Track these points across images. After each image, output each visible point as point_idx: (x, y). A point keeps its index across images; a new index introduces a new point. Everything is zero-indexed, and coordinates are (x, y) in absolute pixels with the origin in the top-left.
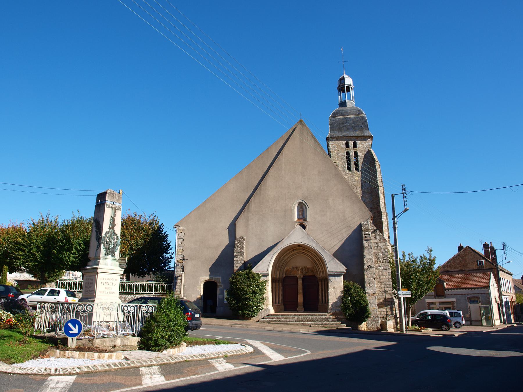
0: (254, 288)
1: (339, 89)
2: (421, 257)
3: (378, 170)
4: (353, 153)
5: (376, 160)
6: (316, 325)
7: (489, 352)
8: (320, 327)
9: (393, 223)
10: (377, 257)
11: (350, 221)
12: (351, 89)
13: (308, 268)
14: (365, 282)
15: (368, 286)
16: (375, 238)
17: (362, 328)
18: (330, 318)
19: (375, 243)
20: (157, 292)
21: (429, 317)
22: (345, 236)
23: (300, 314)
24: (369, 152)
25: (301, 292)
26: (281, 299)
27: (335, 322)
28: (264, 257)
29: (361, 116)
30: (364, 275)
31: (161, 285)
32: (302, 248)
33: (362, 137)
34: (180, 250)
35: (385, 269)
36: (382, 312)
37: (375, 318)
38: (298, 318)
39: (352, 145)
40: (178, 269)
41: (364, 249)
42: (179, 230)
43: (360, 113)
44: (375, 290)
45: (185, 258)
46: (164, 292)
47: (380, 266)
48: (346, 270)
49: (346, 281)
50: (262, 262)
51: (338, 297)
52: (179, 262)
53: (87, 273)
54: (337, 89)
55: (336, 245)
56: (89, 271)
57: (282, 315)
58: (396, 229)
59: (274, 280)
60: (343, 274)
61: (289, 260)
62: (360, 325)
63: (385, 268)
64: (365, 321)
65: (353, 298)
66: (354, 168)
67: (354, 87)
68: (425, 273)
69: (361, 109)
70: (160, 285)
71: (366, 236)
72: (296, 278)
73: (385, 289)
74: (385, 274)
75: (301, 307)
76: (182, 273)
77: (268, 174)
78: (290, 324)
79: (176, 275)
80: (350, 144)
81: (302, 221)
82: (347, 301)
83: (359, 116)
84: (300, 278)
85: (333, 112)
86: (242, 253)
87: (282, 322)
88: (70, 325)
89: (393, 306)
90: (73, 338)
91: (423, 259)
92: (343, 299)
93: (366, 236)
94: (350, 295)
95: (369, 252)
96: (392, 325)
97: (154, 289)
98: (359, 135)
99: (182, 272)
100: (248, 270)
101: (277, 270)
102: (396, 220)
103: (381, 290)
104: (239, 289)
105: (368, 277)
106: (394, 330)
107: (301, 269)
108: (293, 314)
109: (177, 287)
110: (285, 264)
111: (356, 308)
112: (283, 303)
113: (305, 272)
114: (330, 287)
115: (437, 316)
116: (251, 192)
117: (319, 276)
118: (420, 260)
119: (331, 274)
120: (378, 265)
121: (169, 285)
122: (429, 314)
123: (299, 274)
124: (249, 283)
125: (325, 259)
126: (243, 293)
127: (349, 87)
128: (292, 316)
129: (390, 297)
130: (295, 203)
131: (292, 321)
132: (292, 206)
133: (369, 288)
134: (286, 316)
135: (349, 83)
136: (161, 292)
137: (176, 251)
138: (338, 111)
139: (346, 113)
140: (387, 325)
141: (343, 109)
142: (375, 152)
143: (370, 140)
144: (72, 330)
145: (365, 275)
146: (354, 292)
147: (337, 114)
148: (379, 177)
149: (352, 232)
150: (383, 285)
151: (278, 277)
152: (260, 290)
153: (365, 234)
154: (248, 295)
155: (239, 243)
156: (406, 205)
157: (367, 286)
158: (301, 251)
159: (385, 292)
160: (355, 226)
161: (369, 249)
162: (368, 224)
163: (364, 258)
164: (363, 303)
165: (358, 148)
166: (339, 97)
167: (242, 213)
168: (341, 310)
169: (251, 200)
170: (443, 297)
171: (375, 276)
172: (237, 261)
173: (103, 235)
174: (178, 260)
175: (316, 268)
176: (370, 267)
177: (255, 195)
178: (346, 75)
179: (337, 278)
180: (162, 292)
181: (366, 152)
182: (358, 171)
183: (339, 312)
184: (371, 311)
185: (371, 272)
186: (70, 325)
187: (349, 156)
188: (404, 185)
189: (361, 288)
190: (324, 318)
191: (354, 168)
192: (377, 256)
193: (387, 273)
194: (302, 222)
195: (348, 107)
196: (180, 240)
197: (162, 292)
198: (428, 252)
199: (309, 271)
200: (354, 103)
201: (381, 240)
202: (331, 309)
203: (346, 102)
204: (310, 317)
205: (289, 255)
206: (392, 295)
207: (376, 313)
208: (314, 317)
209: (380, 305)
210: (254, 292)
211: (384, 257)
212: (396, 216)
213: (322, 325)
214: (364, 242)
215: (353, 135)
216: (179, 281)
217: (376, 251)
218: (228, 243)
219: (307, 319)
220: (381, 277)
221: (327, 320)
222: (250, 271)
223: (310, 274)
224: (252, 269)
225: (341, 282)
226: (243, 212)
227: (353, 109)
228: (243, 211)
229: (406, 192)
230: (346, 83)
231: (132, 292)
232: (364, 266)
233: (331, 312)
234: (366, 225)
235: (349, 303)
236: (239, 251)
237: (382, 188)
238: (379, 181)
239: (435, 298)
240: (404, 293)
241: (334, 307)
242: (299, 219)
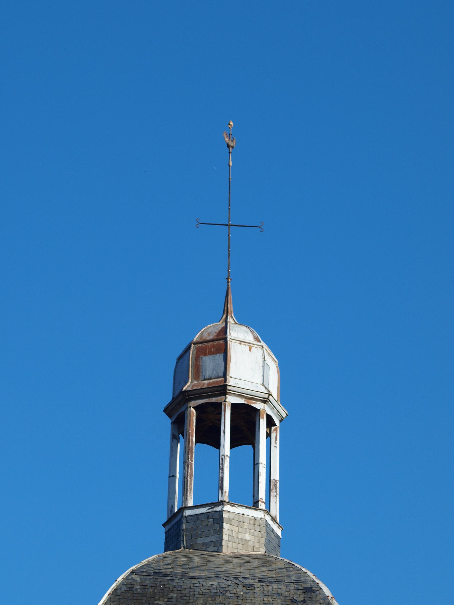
7: (218, 329)
12: (263, 423)
85: (120, 579)
138: (157, 574)
141: (197, 568)
178: (241, 322)
227: (262, 573)
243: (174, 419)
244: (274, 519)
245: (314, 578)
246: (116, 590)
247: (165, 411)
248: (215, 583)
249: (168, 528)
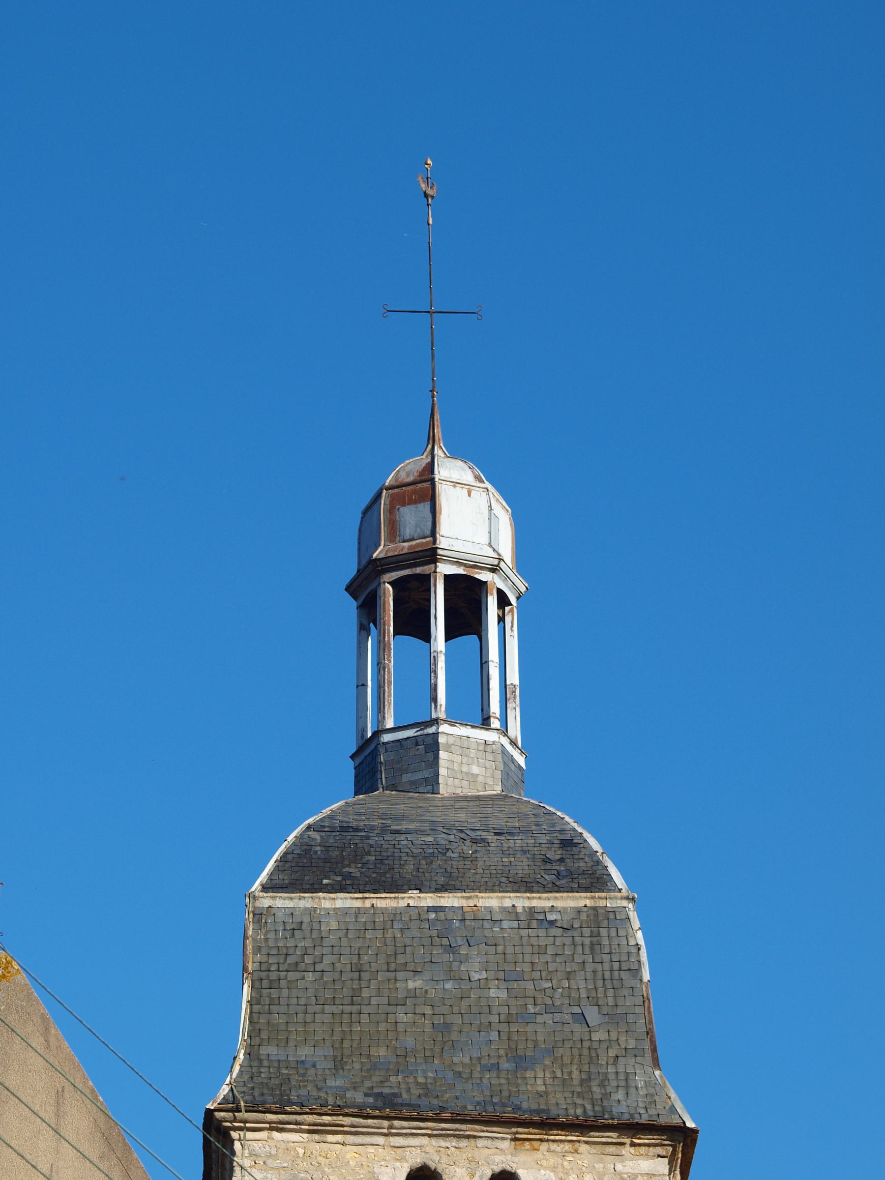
12: (492, 602)
29: (579, 911)
43: (570, 874)
85: (291, 838)
97: (364, 685)
108: (337, 1122)
127: (483, 584)
138: (344, 829)
178: (454, 454)
195: (457, 799)
218: (235, 1147)
227: (499, 821)
243: (362, 598)
244: (513, 743)
245: (575, 825)
246: (285, 854)
247: (347, 589)
248: (430, 839)
249: (358, 760)
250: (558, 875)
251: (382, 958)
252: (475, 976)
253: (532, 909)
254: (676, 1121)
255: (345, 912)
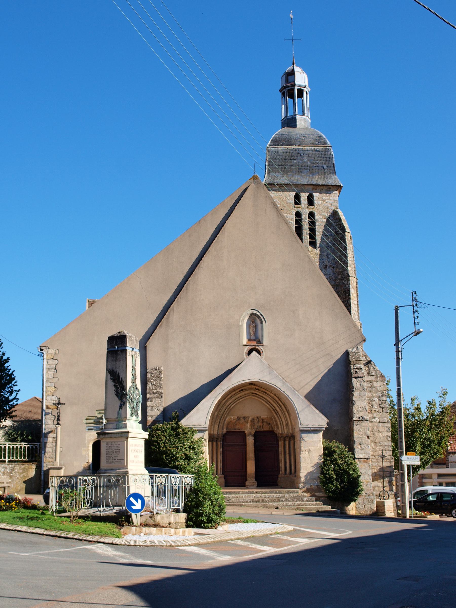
0: (187, 450)
1: (284, 92)
2: (429, 404)
3: (350, 247)
4: (308, 214)
5: (347, 231)
6: (286, 507)
8: (293, 509)
9: (396, 352)
10: (370, 404)
11: (330, 346)
12: (305, 93)
13: (262, 419)
14: (354, 441)
15: (359, 447)
16: (369, 374)
17: (350, 511)
18: (304, 497)
19: (369, 382)
20: (13, 459)
21: (431, 498)
22: (323, 371)
23: (258, 491)
24: (335, 214)
25: (252, 457)
26: (220, 468)
27: (313, 501)
28: (200, 402)
30: (353, 431)
31: (19, 447)
32: (255, 387)
33: (324, 187)
34: (51, 388)
35: (382, 423)
36: (377, 488)
37: (369, 495)
38: (255, 496)
39: (305, 200)
40: (48, 421)
41: (353, 391)
42: (47, 353)
44: (369, 454)
45: (62, 401)
46: (24, 458)
47: (374, 418)
48: (327, 423)
49: (326, 441)
50: (198, 410)
51: (315, 465)
52: (50, 408)
53: (107, 439)
54: (280, 91)
55: (308, 383)
56: (109, 436)
57: (230, 493)
58: (400, 361)
59: (212, 439)
60: (323, 429)
61: (233, 405)
62: (347, 506)
63: (382, 421)
64: (355, 501)
65: (338, 466)
66: (308, 241)
67: (309, 90)
68: (434, 428)
69: (323, 134)
70: (17, 447)
71: (356, 371)
72: (243, 435)
73: (382, 453)
74: (382, 429)
75: (251, 480)
76: (57, 427)
77: (201, 264)
78: (244, 506)
79: (45, 429)
80: (302, 199)
81: (254, 343)
82: (329, 470)
83: (320, 148)
84: (250, 434)
85: (273, 136)
86: (160, 395)
87: (231, 503)
88: (132, 499)
89: (392, 479)
90: (136, 515)
91: (431, 406)
92: (323, 468)
93: (357, 370)
94: (334, 461)
95: (361, 396)
96: (392, 507)
97: (8, 453)
98: (319, 184)
99: (57, 424)
100: (174, 423)
101: (215, 422)
102: (400, 346)
103: (375, 455)
104: (165, 452)
105: (358, 434)
106: (394, 515)
107: (251, 421)
109: (47, 450)
110: (228, 412)
111: (342, 482)
112: (223, 474)
113: (258, 425)
114: (302, 449)
115: (443, 495)
116: (172, 294)
117: (281, 432)
118: (428, 407)
119: (305, 429)
120: (372, 415)
121: (32, 447)
122: (431, 492)
123: (248, 428)
124: (180, 443)
125: (296, 406)
126: (171, 458)
128: (245, 494)
129: (389, 465)
130: (244, 314)
131: (247, 502)
132: (240, 318)
133: (360, 451)
134: (236, 494)
135: (302, 84)
136: (19, 458)
137: (44, 390)
138: (282, 135)
139: (296, 139)
140: (386, 507)
142: (344, 215)
143: (336, 192)
144: (134, 505)
145: (355, 432)
146: (339, 457)
147: (280, 141)
148: (350, 261)
149: (334, 364)
150: (378, 447)
151: (216, 432)
152: (196, 454)
153: (355, 368)
154: (178, 461)
155: (153, 377)
156: (416, 323)
157: (357, 448)
158: (253, 392)
159: (383, 457)
160: (338, 355)
161: (361, 391)
162: (359, 352)
163: (354, 404)
164: (353, 474)
165: (315, 205)
166: (283, 106)
167: (158, 328)
168: (319, 484)
169: (171, 307)
170: (444, 466)
171: (369, 433)
172: (152, 407)
173: (128, 391)
174: (47, 404)
175: (275, 418)
176: (362, 419)
177: (178, 300)
178: (297, 66)
179: (313, 436)
180: (21, 458)
181: (329, 214)
182: (315, 247)
183: (316, 486)
184: (363, 486)
185: (363, 426)
186: (132, 499)
187: (301, 220)
188: (415, 292)
189: (348, 451)
190: (295, 497)
191: (308, 241)
192: (370, 402)
193: (384, 429)
194: (256, 346)
196: (50, 371)
197: (21, 458)
198: (441, 395)
199: (265, 423)
200: (310, 121)
201: (377, 377)
202: (304, 483)
203: (296, 117)
204: (274, 494)
205: (234, 398)
206: (391, 462)
207: (369, 488)
208: (280, 494)
209: (375, 477)
210: (188, 458)
211: (380, 403)
212: (400, 340)
213: (293, 506)
214: (354, 380)
215: (308, 183)
216: (50, 440)
217: (370, 395)
219: (268, 497)
220: (376, 434)
221: (300, 499)
222: (177, 423)
223: (266, 428)
224: (180, 420)
225: (320, 441)
226: (159, 326)
227: (308, 133)
228: (158, 325)
229: (419, 305)
230: (296, 83)
231: (3, 459)
232: (353, 418)
233: (304, 487)
234: (355, 353)
235: (331, 473)
236: (155, 391)
237: (355, 279)
238: (350, 266)
239: (431, 468)
240: (413, 459)
241: (308, 480)
242: (249, 340)
249: (282, 121)
250: (318, 142)
251: (289, 157)
252: (305, 160)
253: (315, 149)
254: (339, 185)
255: (283, 150)
